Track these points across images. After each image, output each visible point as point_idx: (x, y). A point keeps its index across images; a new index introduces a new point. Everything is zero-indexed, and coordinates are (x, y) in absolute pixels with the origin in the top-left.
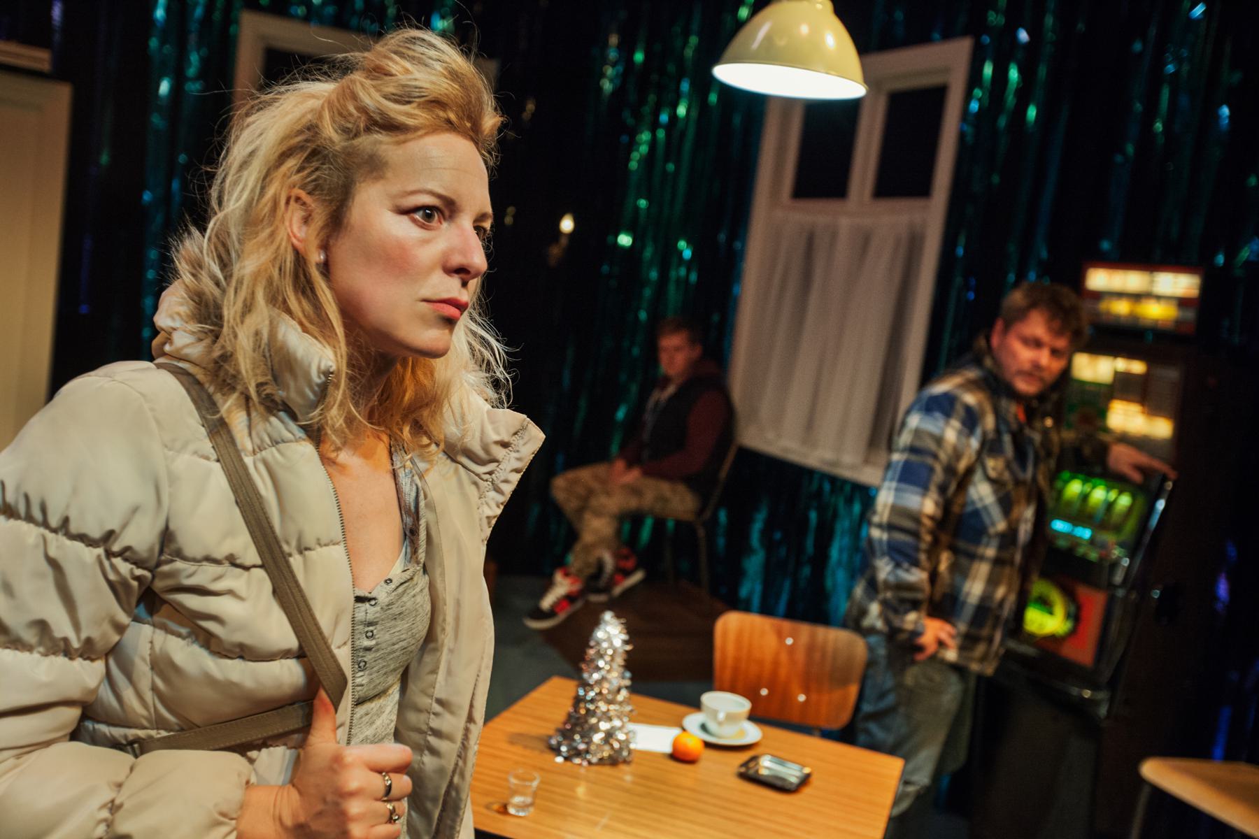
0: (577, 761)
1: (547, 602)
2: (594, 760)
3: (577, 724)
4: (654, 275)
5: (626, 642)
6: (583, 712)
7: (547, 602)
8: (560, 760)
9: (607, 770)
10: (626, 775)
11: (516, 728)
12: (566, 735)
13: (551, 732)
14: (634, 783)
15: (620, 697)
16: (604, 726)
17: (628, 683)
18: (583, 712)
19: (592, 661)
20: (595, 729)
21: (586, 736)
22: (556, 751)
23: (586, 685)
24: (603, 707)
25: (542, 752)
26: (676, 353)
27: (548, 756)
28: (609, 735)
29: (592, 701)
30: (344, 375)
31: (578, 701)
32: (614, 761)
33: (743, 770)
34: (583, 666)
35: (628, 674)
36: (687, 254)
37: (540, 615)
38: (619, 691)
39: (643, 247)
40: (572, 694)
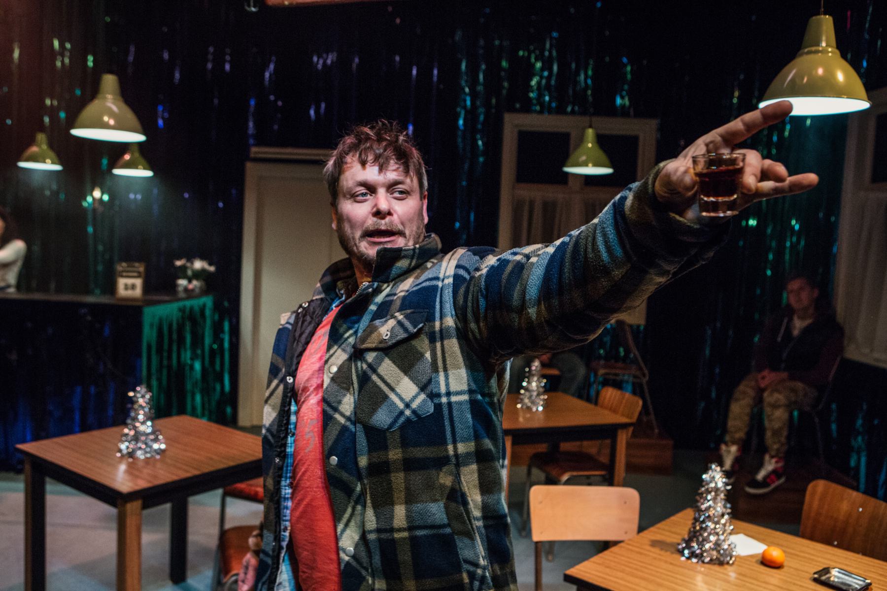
0: (694, 560)
1: (760, 476)
2: (707, 560)
3: (695, 535)
4: (774, 244)
5: (726, 484)
6: (698, 528)
7: (760, 476)
8: (683, 559)
9: (716, 568)
10: (731, 573)
11: (658, 537)
12: (688, 542)
13: (679, 541)
14: (737, 578)
15: (723, 521)
16: (713, 538)
17: (729, 511)
18: (698, 528)
19: (702, 494)
20: (706, 540)
21: (701, 544)
22: (681, 553)
23: (699, 511)
24: (711, 525)
25: (672, 553)
26: (797, 293)
27: (677, 556)
28: (717, 544)
29: (703, 522)
30: (208, 322)
31: (696, 520)
32: (720, 562)
33: (816, 576)
34: (698, 498)
35: (729, 505)
36: (797, 227)
37: (756, 484)
38: (723, 515)
39: (766, 227)
40: (693, 516)
